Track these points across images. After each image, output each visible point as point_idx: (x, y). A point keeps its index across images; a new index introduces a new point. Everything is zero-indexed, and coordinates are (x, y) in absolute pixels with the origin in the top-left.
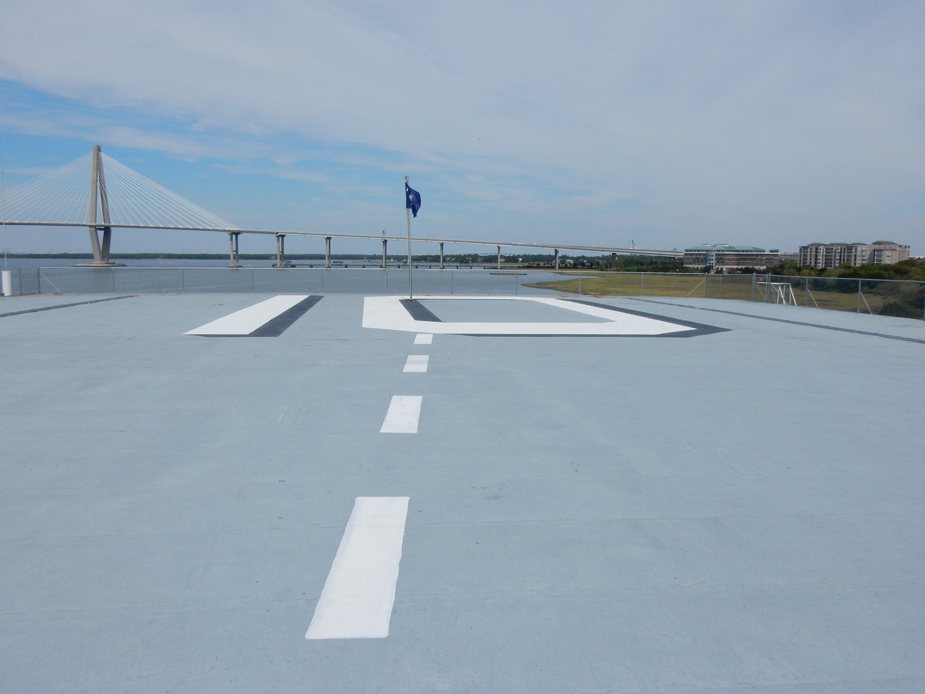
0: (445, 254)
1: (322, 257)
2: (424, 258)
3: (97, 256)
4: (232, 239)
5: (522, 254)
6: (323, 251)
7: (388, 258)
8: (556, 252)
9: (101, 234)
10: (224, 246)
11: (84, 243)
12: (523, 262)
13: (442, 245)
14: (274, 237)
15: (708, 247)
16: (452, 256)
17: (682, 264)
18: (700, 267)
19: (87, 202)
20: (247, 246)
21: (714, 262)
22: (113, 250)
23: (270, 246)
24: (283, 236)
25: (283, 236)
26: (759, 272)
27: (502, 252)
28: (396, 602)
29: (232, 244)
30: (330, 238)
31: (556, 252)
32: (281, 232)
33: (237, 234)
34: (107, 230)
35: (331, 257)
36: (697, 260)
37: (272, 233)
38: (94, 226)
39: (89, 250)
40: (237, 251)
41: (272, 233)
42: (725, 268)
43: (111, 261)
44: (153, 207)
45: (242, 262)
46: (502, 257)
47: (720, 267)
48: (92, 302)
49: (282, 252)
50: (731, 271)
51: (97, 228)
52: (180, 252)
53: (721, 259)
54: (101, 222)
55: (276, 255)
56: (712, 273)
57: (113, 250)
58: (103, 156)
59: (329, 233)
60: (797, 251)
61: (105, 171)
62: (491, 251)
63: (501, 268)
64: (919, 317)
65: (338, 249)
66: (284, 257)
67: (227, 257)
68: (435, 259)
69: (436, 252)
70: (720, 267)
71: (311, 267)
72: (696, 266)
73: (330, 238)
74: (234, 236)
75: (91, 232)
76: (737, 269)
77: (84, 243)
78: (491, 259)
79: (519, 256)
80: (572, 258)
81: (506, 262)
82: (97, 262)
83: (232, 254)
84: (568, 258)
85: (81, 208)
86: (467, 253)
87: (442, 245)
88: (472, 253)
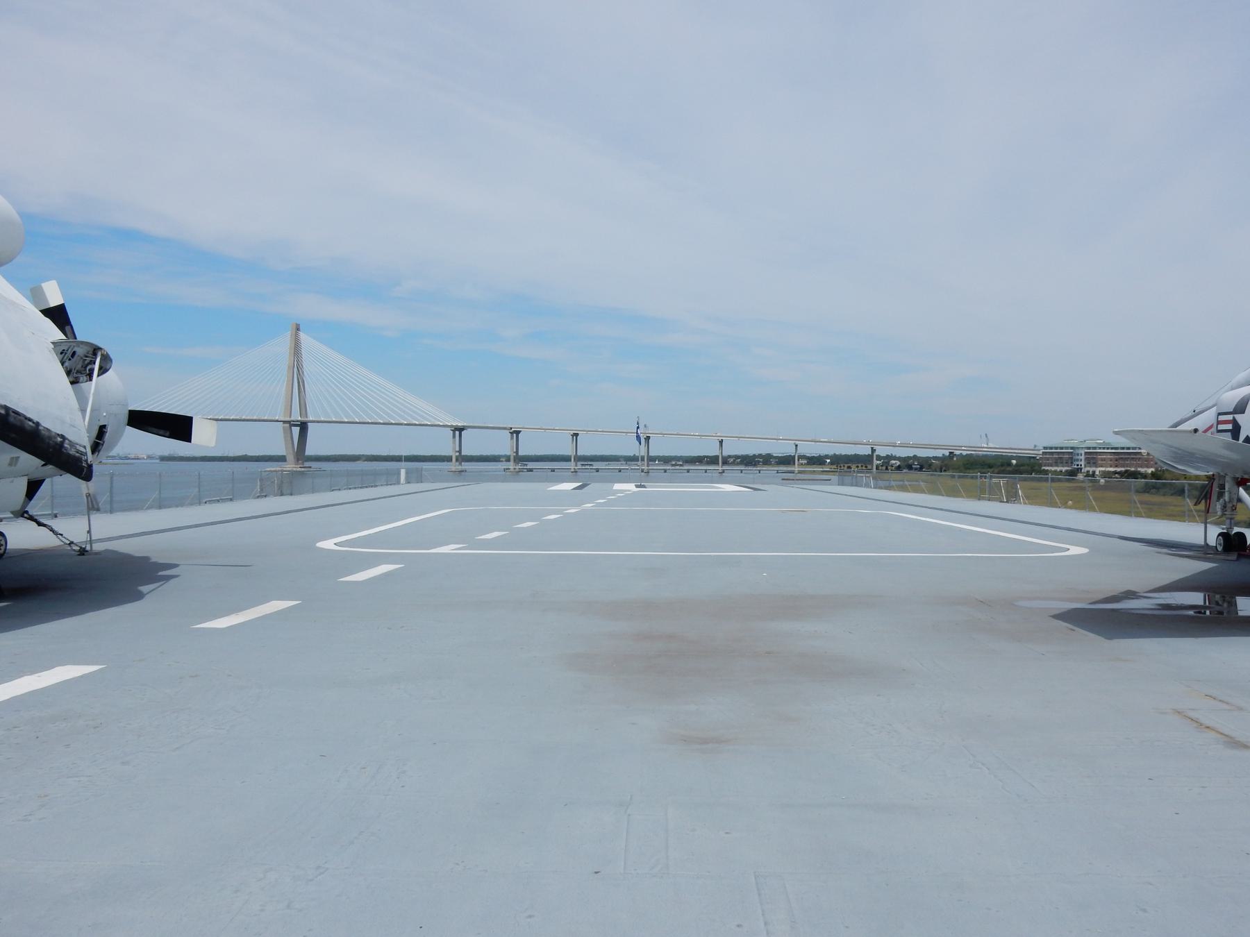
0: (725, 453)
1: (566, 459)
2: (699, 460)
3: (290, 458)
4: (454, 436)
5: (831, 453)
6: (568, 450)
7: (652, 459)
8: (873, 450)
9: (296, 430)
10: (446, 446)
11: (275, 442)
12: (831, 463)
13: (721, 442)
15: (1075, 443)
16: (737, 457)
17: (1041, 465)
18: (1064, 469)
19: (281, 388)
21: (1083, 463)
22: (309, 451)
23: (503, 446)
24: (518, 433)
25: (518, 433)
26: (1145, 476)
27: (801, 451)
28: (325, 491)
30: (576, 435)
31: (873, 450)
32: (516, 427)
33: (461, 429)
34: (303, 427)
35: (579, 459)
36: (1058, 462)
39: (280, 451)
40: (460, 451)
42: (1098, 470)
43: (307, 464)
44: (357, 397)
46: (801, 457)
47: (1091, 470)
49: (517, 452)
50: (1105, 475)
51: (291, 424)
52: (385, 454)
53: (1092, 458)
54: (296, 417)
56: (1080, 477)
58: (302, 335)
59: (575, 428)
62: (788, 450)
63: (800, 472)
64: (6, 408)
65: (730, 450)
66: (519, 459)
67: (449, 459)
68: (713, 460)
69: (713, 451)
70: (1091, 470)
72: (1058, 469)
73: (576, 435)
74: (1230, 427)
76: (1115, 473)
77: (275, 442)
78: (787, 461)
79: (827, 457)
80: (899, 459)
81: (808, 464)
82: (290, 466)
83: (454, 455)
84: (895, 458)
86: (757, 453)
87: (721, 442)
88: (764, 452)
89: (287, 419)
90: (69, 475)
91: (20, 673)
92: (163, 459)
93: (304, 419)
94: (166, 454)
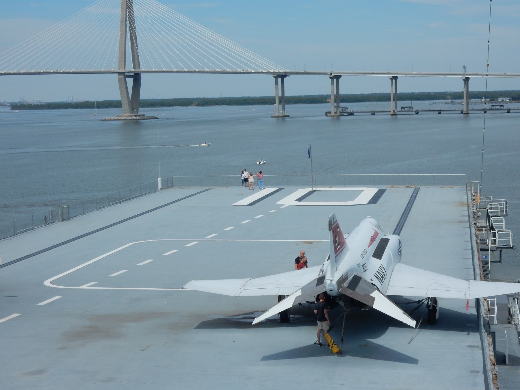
3: (126, 105)
4: (277, 83)
9: (130, 81)
10: (268, 88)
11: (111, 90)
14: (327, 78)
19: (114, 33)
20: (294, 87)
22: (144, 95)
23: (324, 87)
24: (338, 77)
25: (338, 77)
29: (277, 89)
30: (396, 78)
32: (336, 71)
33: (283, 76)
34: (137, 77)
37: (325, 74)
38: (123, 73)
41: (325, 74)
45: (290, 109)
48: (200, 192)
51: (125, 75)
54: (130, 68)
55: (329, 97)
57: (144, 95)
59: (394, 71)
60: (313, 299)
61: (135, 8)
65: (403, 88)
71: (373, 114)
73: (396, 78)
74: (280, 79)
75: (119, 80)
77: (111, 90)
82: (125, 114)
85: (105, 50)
89: (122, 71)
90: (233, 295)
91: (68, 270)
92: (15, 107)
93: (137, 70)
94: (16, 100)
